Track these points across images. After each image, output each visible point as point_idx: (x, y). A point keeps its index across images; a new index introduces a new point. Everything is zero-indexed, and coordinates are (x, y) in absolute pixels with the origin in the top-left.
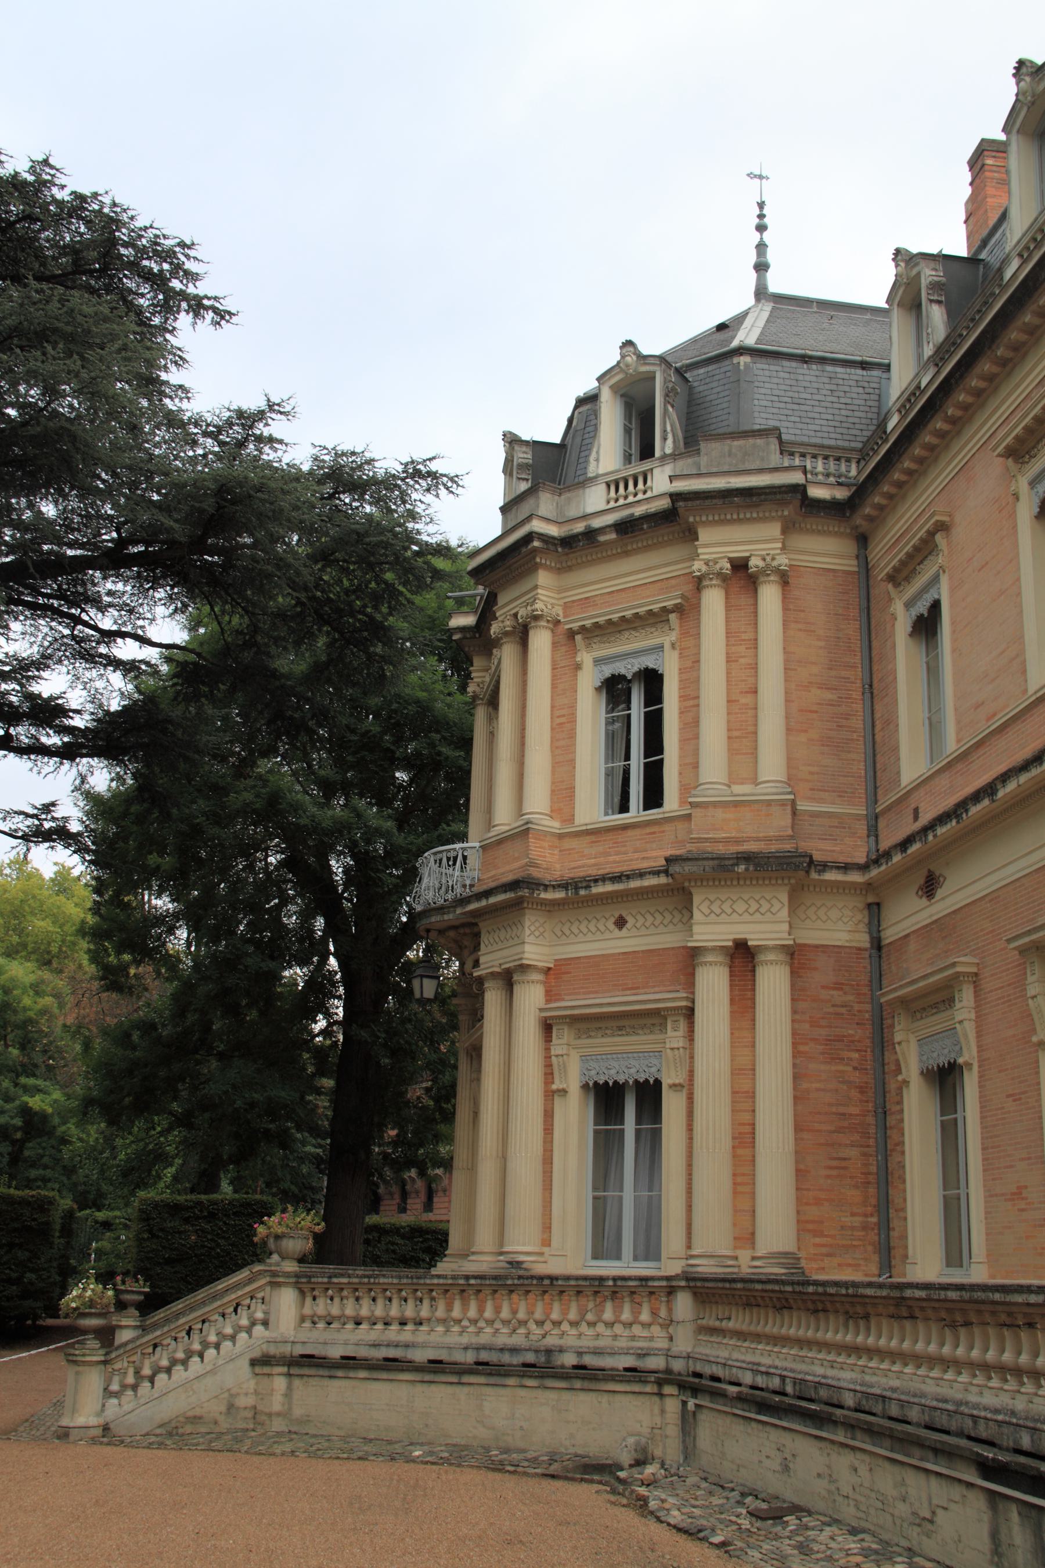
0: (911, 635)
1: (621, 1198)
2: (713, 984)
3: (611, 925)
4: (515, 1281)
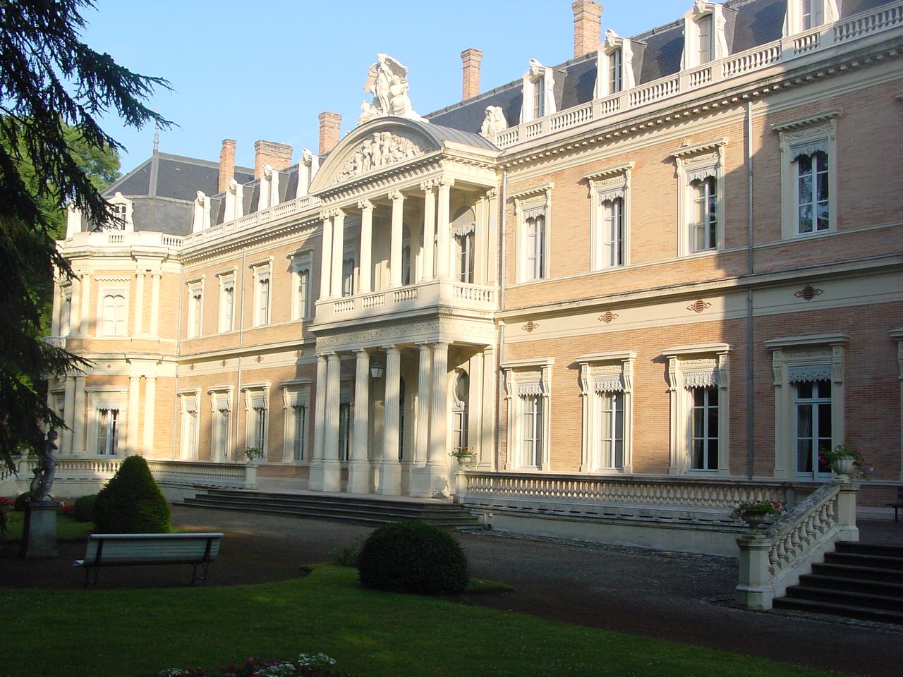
1: (811, 441)
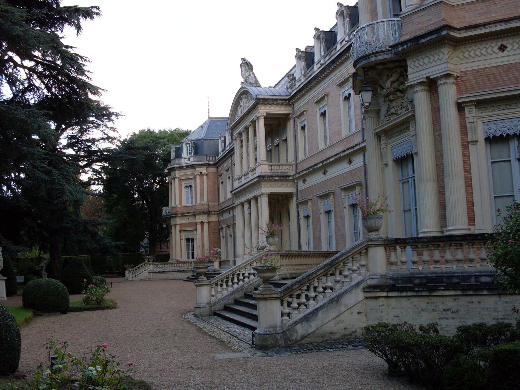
2: (199, 227)
3: (496, 49)
4: (178, 262)
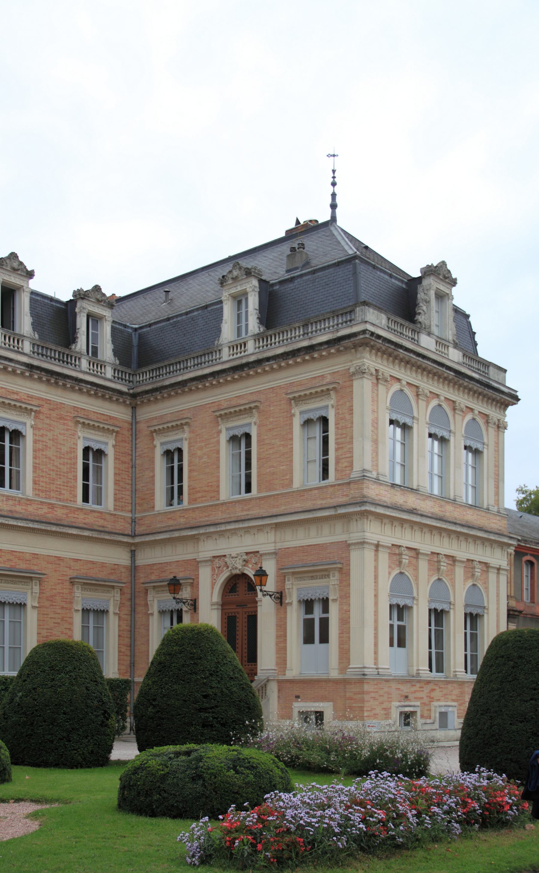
0: (162, 455)
